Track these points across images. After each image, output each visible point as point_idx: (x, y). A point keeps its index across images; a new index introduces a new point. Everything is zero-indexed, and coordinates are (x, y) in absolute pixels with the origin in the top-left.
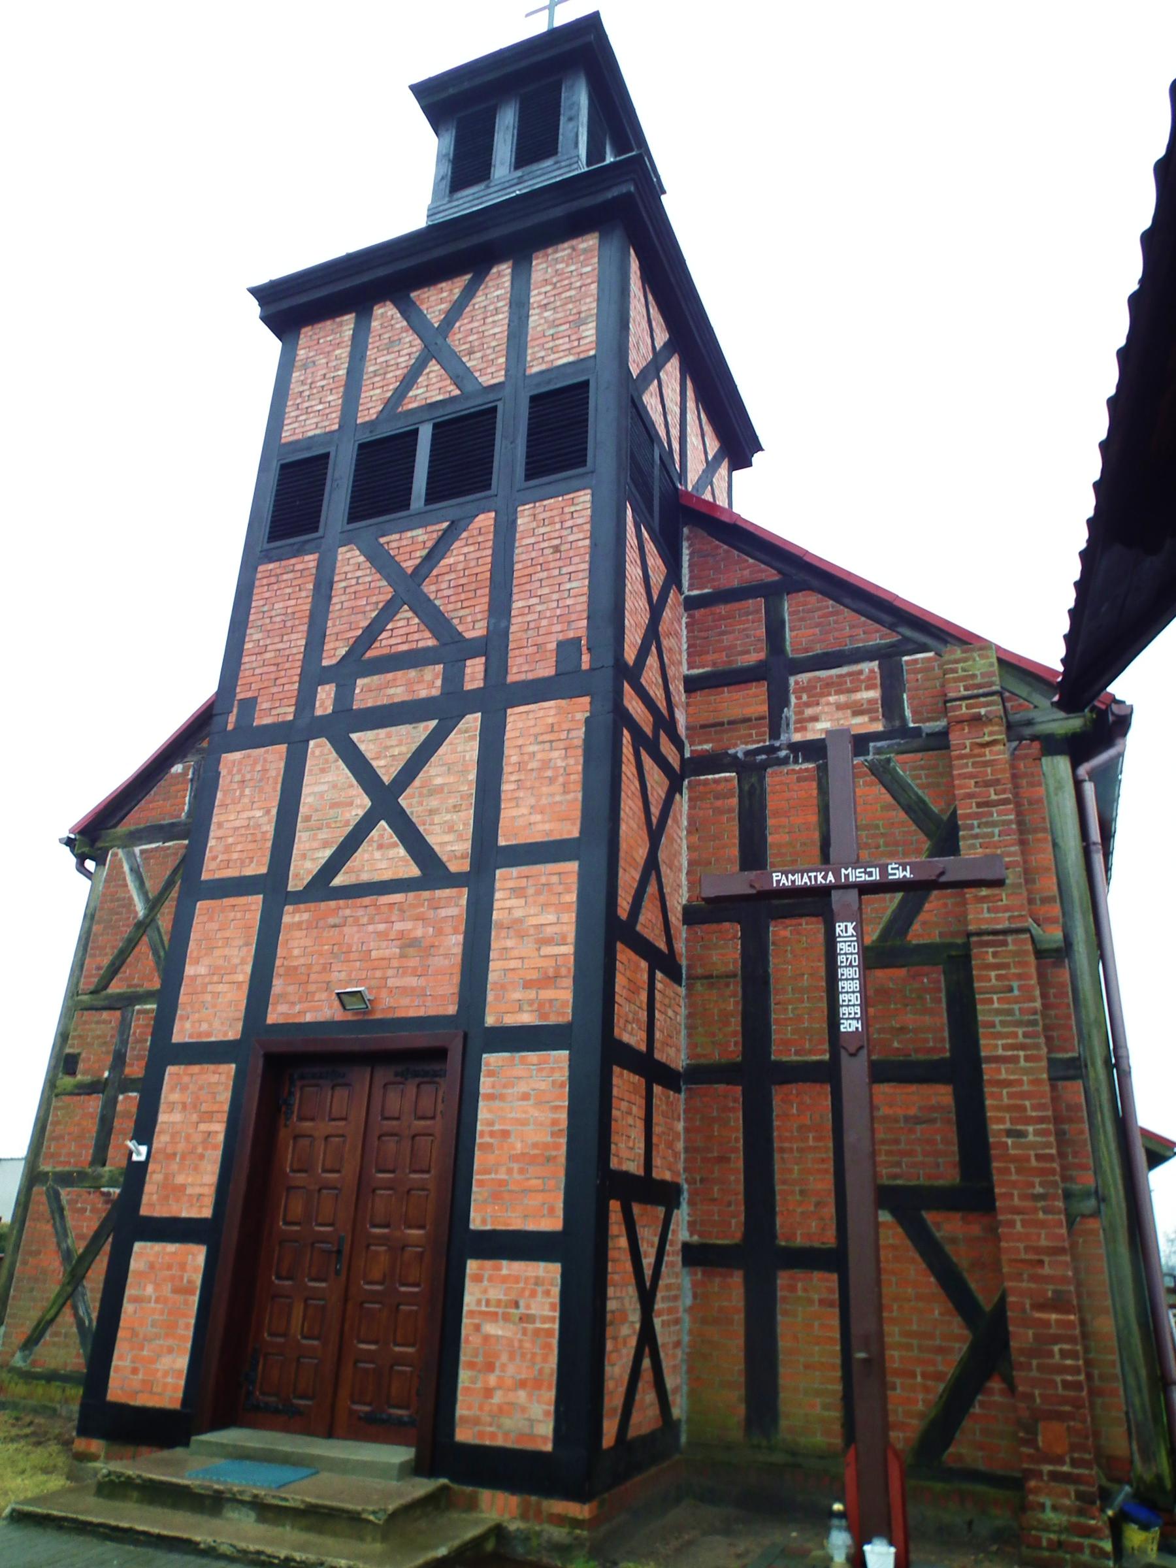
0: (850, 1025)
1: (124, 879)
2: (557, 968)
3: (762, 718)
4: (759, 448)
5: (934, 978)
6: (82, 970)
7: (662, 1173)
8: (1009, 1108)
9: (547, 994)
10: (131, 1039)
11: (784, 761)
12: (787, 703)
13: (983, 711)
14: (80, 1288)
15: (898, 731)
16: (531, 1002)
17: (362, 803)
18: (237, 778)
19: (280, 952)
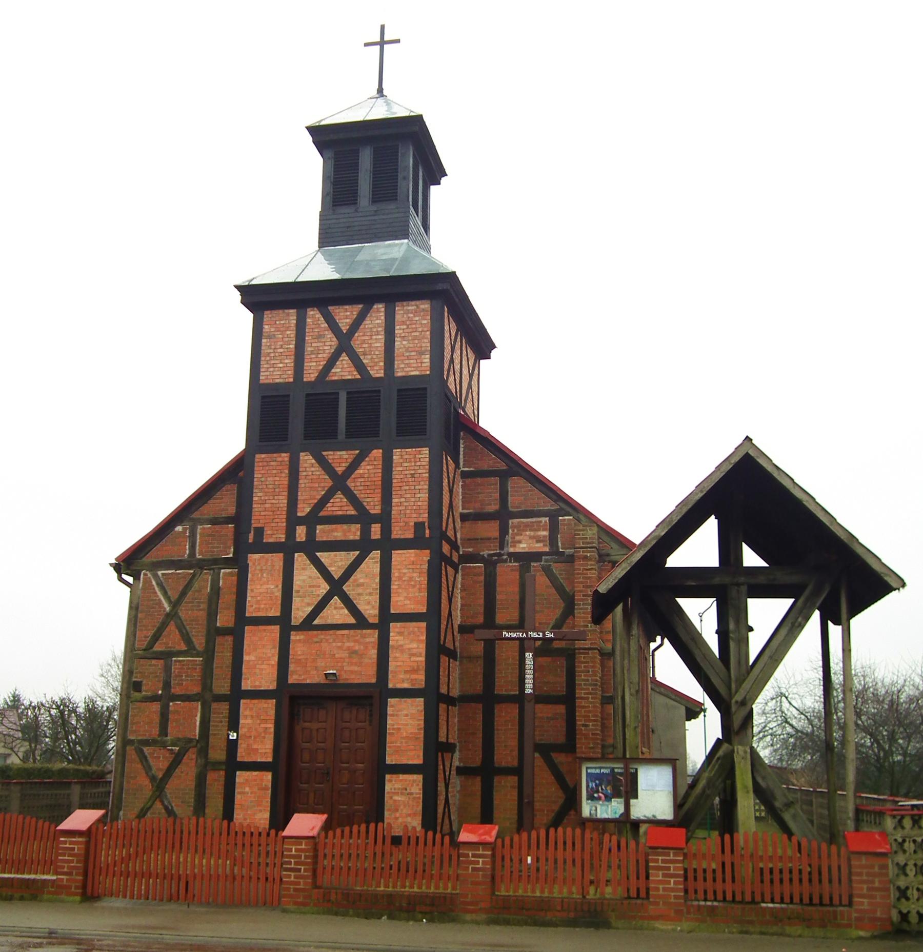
0: (529, 690)
1: (154, 589)
2: (418, 666)
3: (496, 539)
4: (494, 347)
5: (561, 662)
6: (135, 637)
7: (451, 741)
8: (585, 716)
9: (413, 676)
10: (173, 675)
11: (505, 561)
12: (507, 533)
13: (589, 554)
14: (163, 793)
15: (554, 552)
16: (408, 679)
17: (324, 588)
18: (258, 568)
19: (291, 652)
